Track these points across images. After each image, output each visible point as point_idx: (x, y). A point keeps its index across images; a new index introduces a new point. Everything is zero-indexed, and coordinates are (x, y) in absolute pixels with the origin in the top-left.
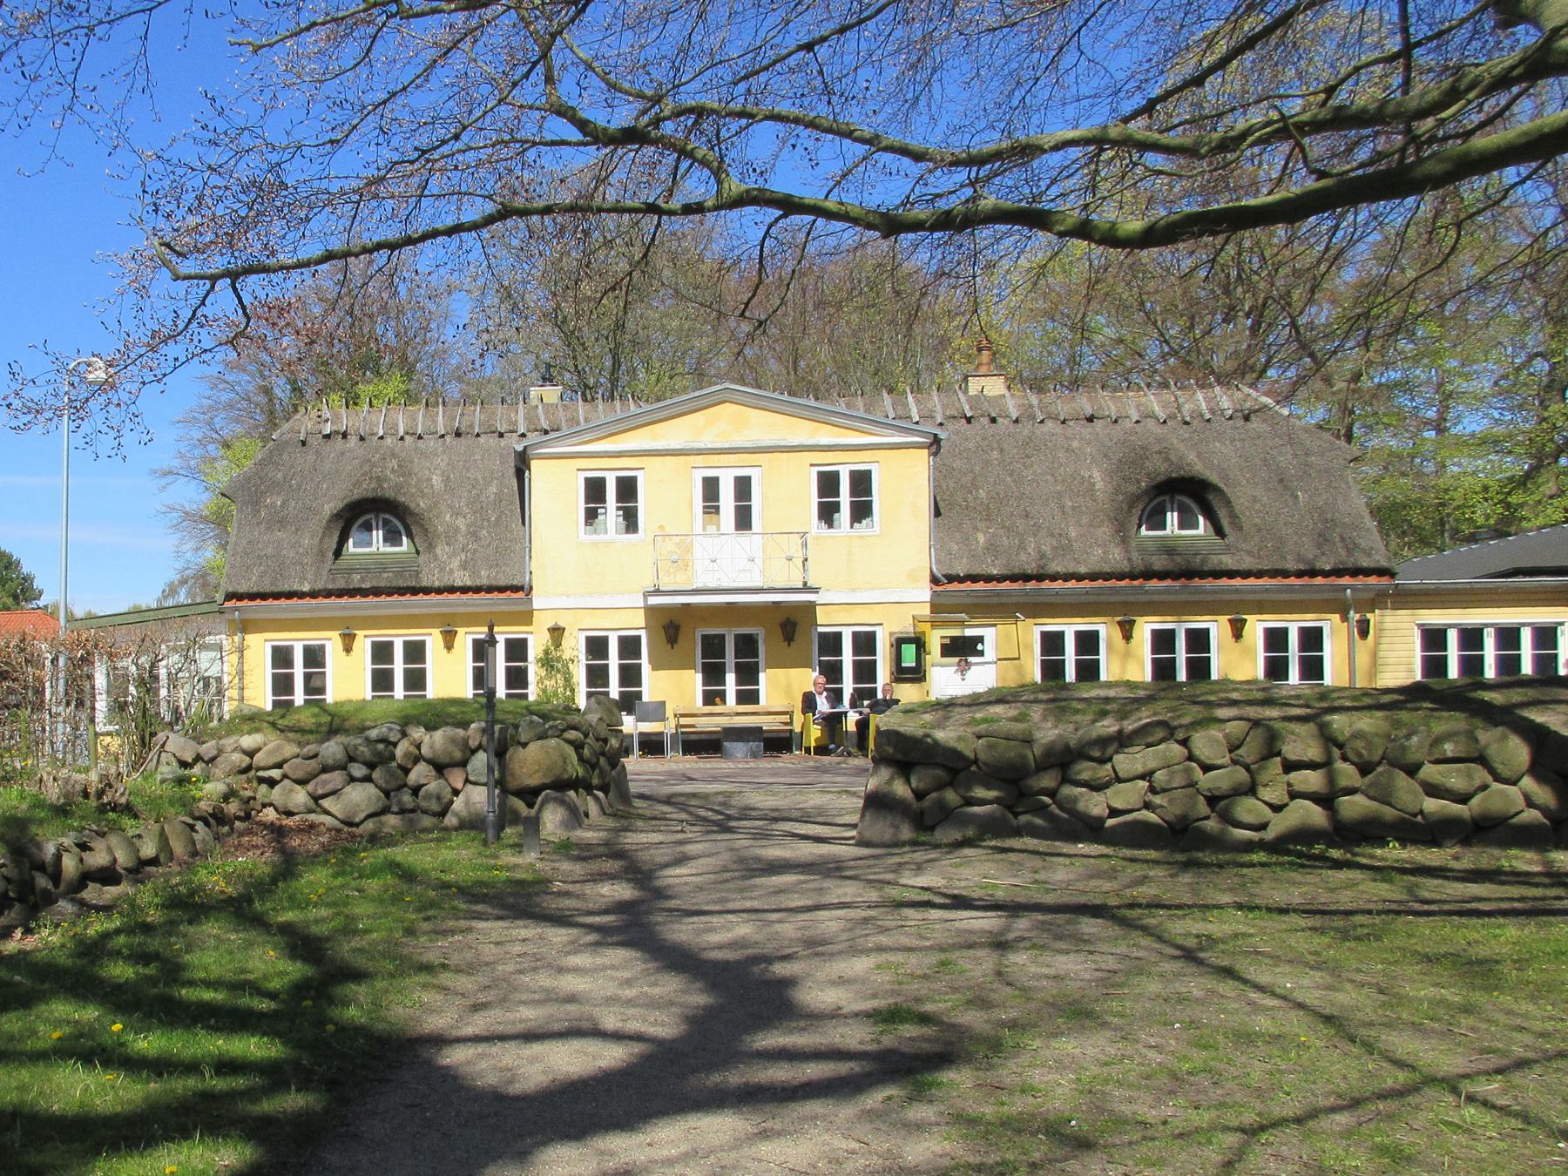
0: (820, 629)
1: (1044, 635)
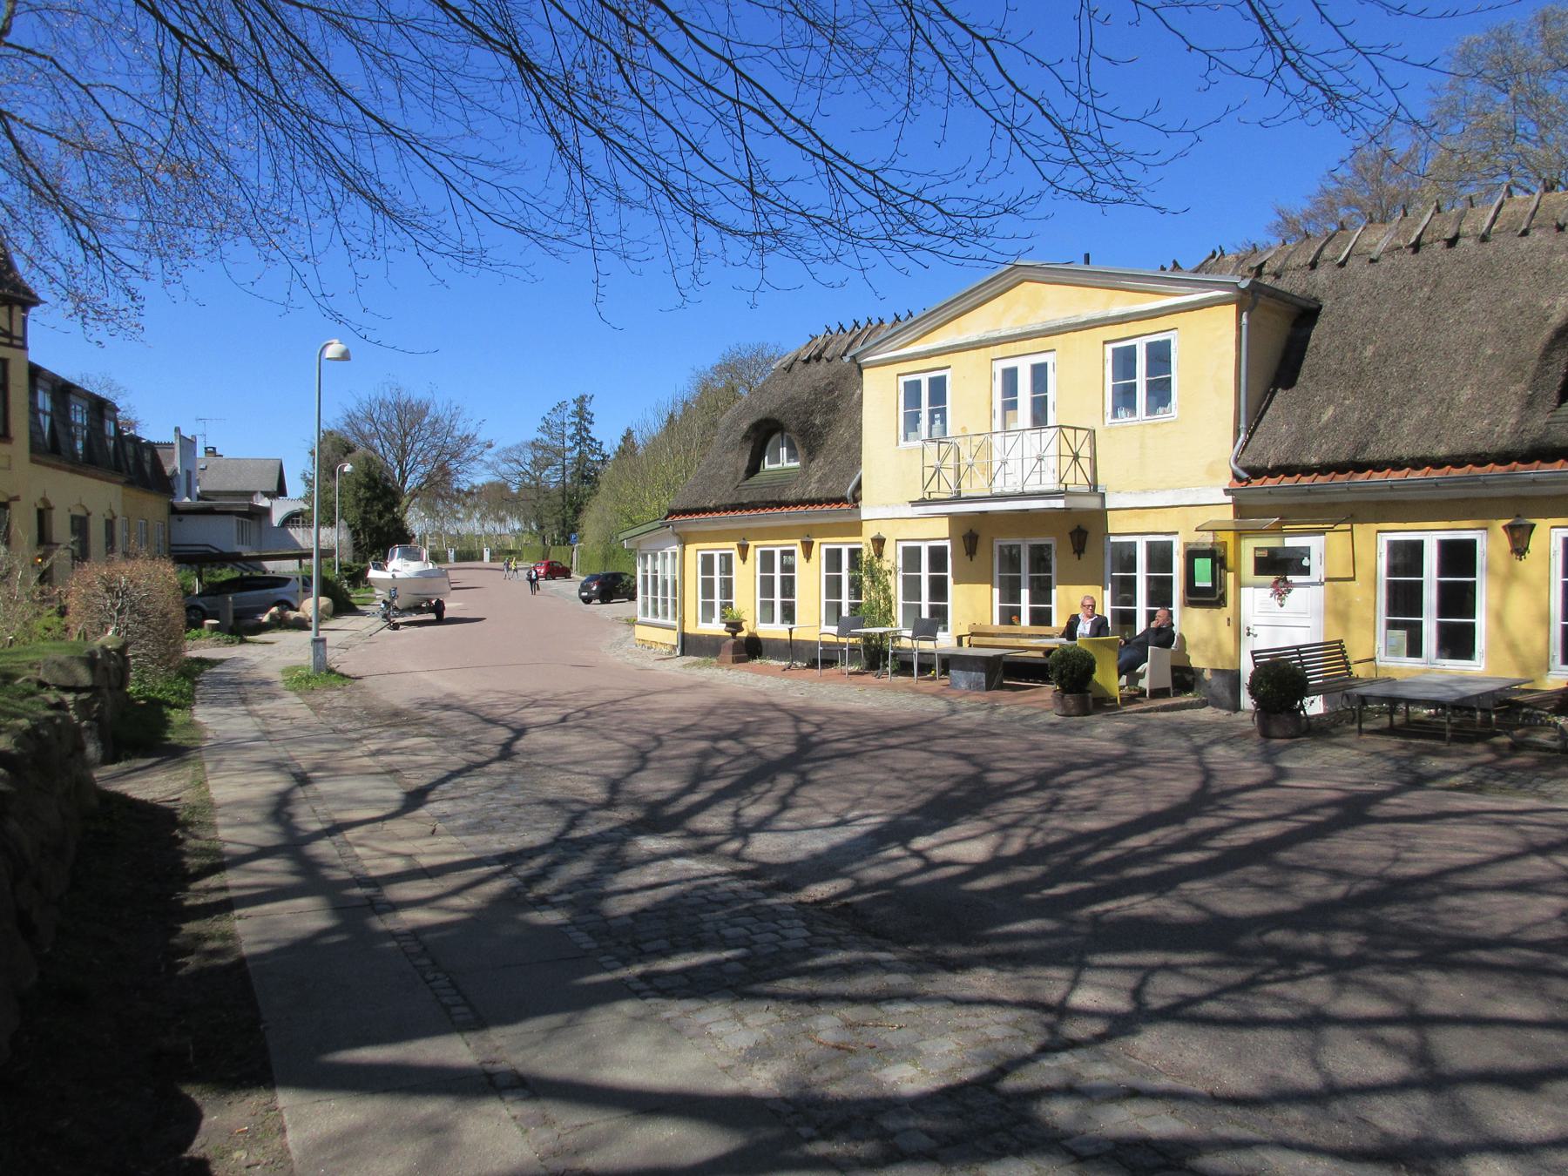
0: (1113, 539)
1: (1394, 547)
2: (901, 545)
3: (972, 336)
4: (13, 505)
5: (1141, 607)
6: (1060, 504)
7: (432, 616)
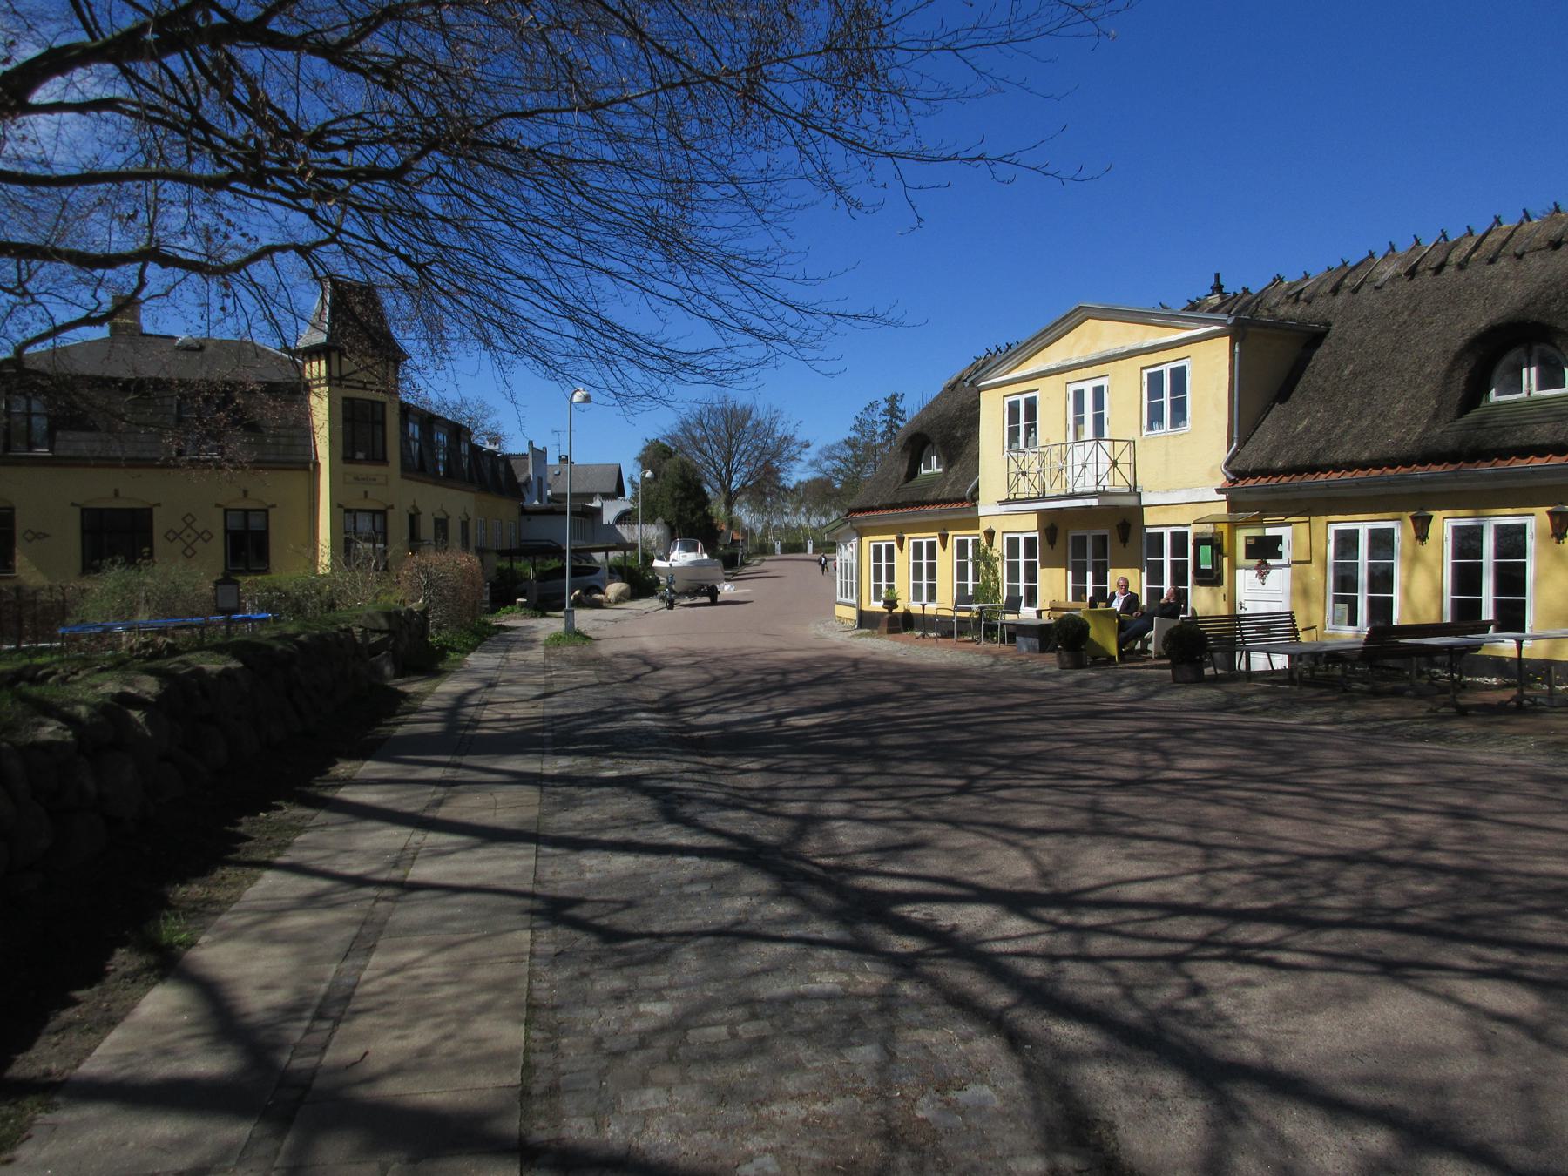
0: (1148, 530)
2: (1006, 536)
3: (1051, 365)
4: (390, 512)
5: (1167, 586)
6: (1094, 502)
7: (707, 600)
